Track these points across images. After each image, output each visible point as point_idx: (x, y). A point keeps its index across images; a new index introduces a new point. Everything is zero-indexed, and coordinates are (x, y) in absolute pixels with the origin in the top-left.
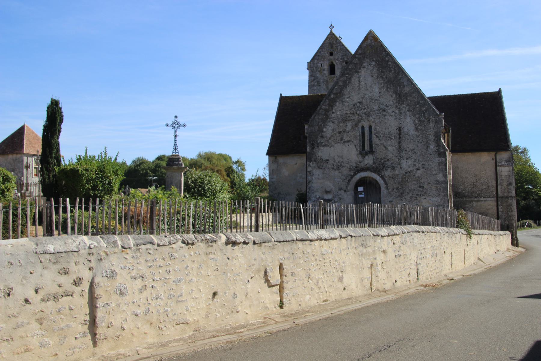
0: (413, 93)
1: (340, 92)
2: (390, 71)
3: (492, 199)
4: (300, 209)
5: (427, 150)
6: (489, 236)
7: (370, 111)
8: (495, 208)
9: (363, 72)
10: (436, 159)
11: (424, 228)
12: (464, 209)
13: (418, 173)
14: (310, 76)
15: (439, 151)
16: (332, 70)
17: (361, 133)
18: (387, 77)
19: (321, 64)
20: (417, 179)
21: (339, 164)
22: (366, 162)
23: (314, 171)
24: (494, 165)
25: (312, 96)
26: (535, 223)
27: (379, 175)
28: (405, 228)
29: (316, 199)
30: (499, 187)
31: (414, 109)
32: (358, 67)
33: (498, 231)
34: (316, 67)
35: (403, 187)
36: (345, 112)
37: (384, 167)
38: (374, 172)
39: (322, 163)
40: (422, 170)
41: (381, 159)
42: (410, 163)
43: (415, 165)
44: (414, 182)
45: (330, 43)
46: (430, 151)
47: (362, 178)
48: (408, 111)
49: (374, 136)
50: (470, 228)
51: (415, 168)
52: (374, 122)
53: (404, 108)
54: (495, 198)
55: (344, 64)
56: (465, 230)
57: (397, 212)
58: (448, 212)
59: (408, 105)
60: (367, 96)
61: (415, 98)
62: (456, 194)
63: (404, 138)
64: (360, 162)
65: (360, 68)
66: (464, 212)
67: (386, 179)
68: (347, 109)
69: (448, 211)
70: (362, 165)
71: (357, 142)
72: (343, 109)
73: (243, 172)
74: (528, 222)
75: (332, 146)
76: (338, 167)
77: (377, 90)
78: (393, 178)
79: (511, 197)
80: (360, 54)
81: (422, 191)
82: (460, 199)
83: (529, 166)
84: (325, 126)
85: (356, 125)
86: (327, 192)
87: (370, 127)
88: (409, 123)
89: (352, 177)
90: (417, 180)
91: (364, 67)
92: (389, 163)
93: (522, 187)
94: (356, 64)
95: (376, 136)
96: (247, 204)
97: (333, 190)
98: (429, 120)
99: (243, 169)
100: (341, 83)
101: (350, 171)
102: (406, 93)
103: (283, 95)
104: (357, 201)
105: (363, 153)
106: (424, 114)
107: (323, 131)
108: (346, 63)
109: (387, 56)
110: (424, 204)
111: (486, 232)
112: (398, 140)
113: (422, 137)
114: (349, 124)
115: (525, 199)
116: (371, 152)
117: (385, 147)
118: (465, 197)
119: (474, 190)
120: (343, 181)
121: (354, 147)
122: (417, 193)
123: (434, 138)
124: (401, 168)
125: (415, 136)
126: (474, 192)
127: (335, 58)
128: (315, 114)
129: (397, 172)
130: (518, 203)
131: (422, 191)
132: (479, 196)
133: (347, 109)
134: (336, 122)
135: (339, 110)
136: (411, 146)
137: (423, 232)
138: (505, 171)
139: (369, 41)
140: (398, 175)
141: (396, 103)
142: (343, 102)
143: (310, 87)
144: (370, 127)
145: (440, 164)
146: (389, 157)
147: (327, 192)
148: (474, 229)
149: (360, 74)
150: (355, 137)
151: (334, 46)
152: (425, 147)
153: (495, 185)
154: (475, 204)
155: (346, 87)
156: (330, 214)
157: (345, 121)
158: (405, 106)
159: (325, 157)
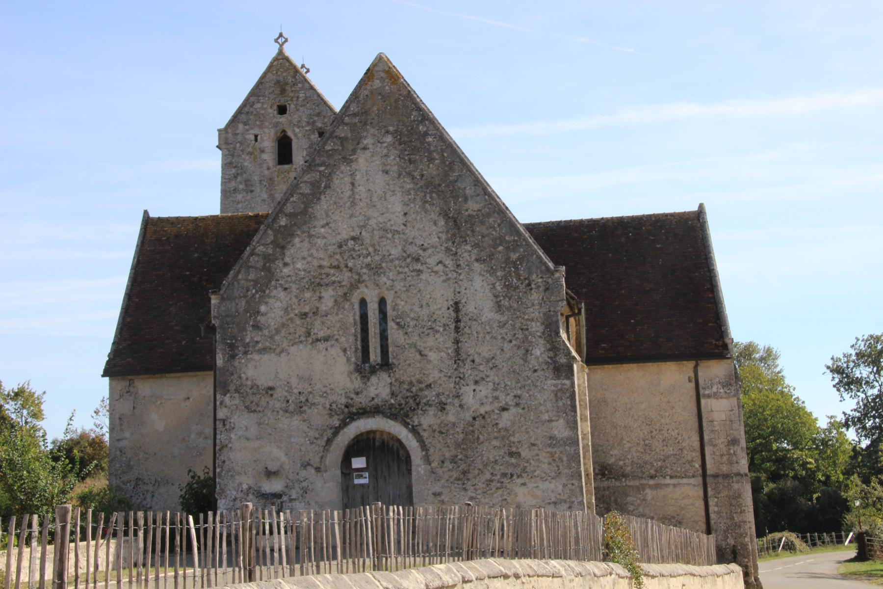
0: (489, 215)
1: (305, 212)
2: (431, 160)
4: (188, 530)
5: (525, 361)
6: (689, 580)
7: (382, 260)
8: (701, 504)
9: (362, 161)
10: (549, 382)
11: (519, 565)
12: (623, 509)
14: (227, 165)
15: (555, 362)
16: (284, 151)
17: (358, 318)
18: (422, 176)
19: (256, 136)
20: (503, 433)
21: (303, 399)
22: (372, 392)
23: (235, 419)
24: (693, 392)
25: (231, 218)
26: (804, 538)
27: (406, 425)
28: (471, 568)
29: (240, 495)
30: (708, 450)
31: (491, 256)
32: (351, 147)
33: (710, 564)
34: (241, 143)
35: (466, 456)
36: (316, 263)
37: (418, 404)
38: (394, 417)
39: (257, 398)
40: (513, 410)
41: (411, 383)
42: (484, 393)
43: (497, 398)
45: (278, 83)
46: (533, 363)
47: (362, 434)
48: (477, 260)
49: (391, 325)
50: (637, 560)
51: (496, 405)
52: (392, 288)
53: (467, 253)
54: (700, 480)
55: (315, 137)
56: (626, 566)
57: (449, 527)
58: (579, 519)
59: (476, 245)
60: (372, 222)
61: (494, 228)
62: (603, 471)
63: (467, 330)
64: (357, 394)
65: (354, 151)
66: (620, 519)
67: (425, 435)
68: (321, 254)
69: (583, 518)
70: (362, 400)
71: (350, 339)
72: (311, 255)
73: (35, 422)
74: (786, 536)
75: (282, 351)
76: (301, 408)
77: (399, 208)
78: (441, 432)
79: (738, 474)
80: (355, 115)
81: (516, 466)
82: (614, 483)
83: (782, 392)
84: (262, 300)
85: (346, 297)
86: (270, 474)
87: (382, 302)
88: (479, 293)
89: (337, 431)
90: (503, 438)
91: (365, 148)
92: (430, 395)
93: (767, 447)
94: (343, 140)
95: (398, 324)
96: (30, 526)
97: (287, 467)
98: (529, 285)
99: (37, 415)
100: (306, 189)
101: (331, 416)
103: (153, 214)
104: (351, 498)
105: (365, 368)
106: (517, 268)
107: (258, 312)
108: (321, 134)
109: (422, 121)
110: (520, 499)
111: (680, 567)
112: (453, 335)
113: (513, 326)
114: (328, 295)
115: (774, 477)
116: (386, 364)
118: (624, 475)
119: (647, 458)
120: (312, 443)
121: (341, 354)
122: (503, 469)
123: (541, 329)
124: (461, 406)
125: (495, 325)
126: (646, 463)
127: (290, 122)
128: (236, 268)
129: (451, 418)
130: (756, 489)
131: (513, 466)
132: (659, 473)
133: (321, 254)
134: (294, 287)
135: (302, 257)
136: (485, 350)
137: (517, 576)
138: (719, 409)
139: (377, 83)
140: (454, 424)
141: (447, 240)
142: (310, 236)
143: (226, 194)
144: (382, 302)
145: (558, 394)
146: (431, 380)
147: (270, 474)
148: (649, 561)
149: (354, 166)
150: (344, 327)
151: (288, 88)
152: (521, 352)
153: (697, 444)
154: (649, 494)
155: (319, 199)
156: (271, 533)
157: (317, 285)
158: (468, 248)
159: (264, 381)
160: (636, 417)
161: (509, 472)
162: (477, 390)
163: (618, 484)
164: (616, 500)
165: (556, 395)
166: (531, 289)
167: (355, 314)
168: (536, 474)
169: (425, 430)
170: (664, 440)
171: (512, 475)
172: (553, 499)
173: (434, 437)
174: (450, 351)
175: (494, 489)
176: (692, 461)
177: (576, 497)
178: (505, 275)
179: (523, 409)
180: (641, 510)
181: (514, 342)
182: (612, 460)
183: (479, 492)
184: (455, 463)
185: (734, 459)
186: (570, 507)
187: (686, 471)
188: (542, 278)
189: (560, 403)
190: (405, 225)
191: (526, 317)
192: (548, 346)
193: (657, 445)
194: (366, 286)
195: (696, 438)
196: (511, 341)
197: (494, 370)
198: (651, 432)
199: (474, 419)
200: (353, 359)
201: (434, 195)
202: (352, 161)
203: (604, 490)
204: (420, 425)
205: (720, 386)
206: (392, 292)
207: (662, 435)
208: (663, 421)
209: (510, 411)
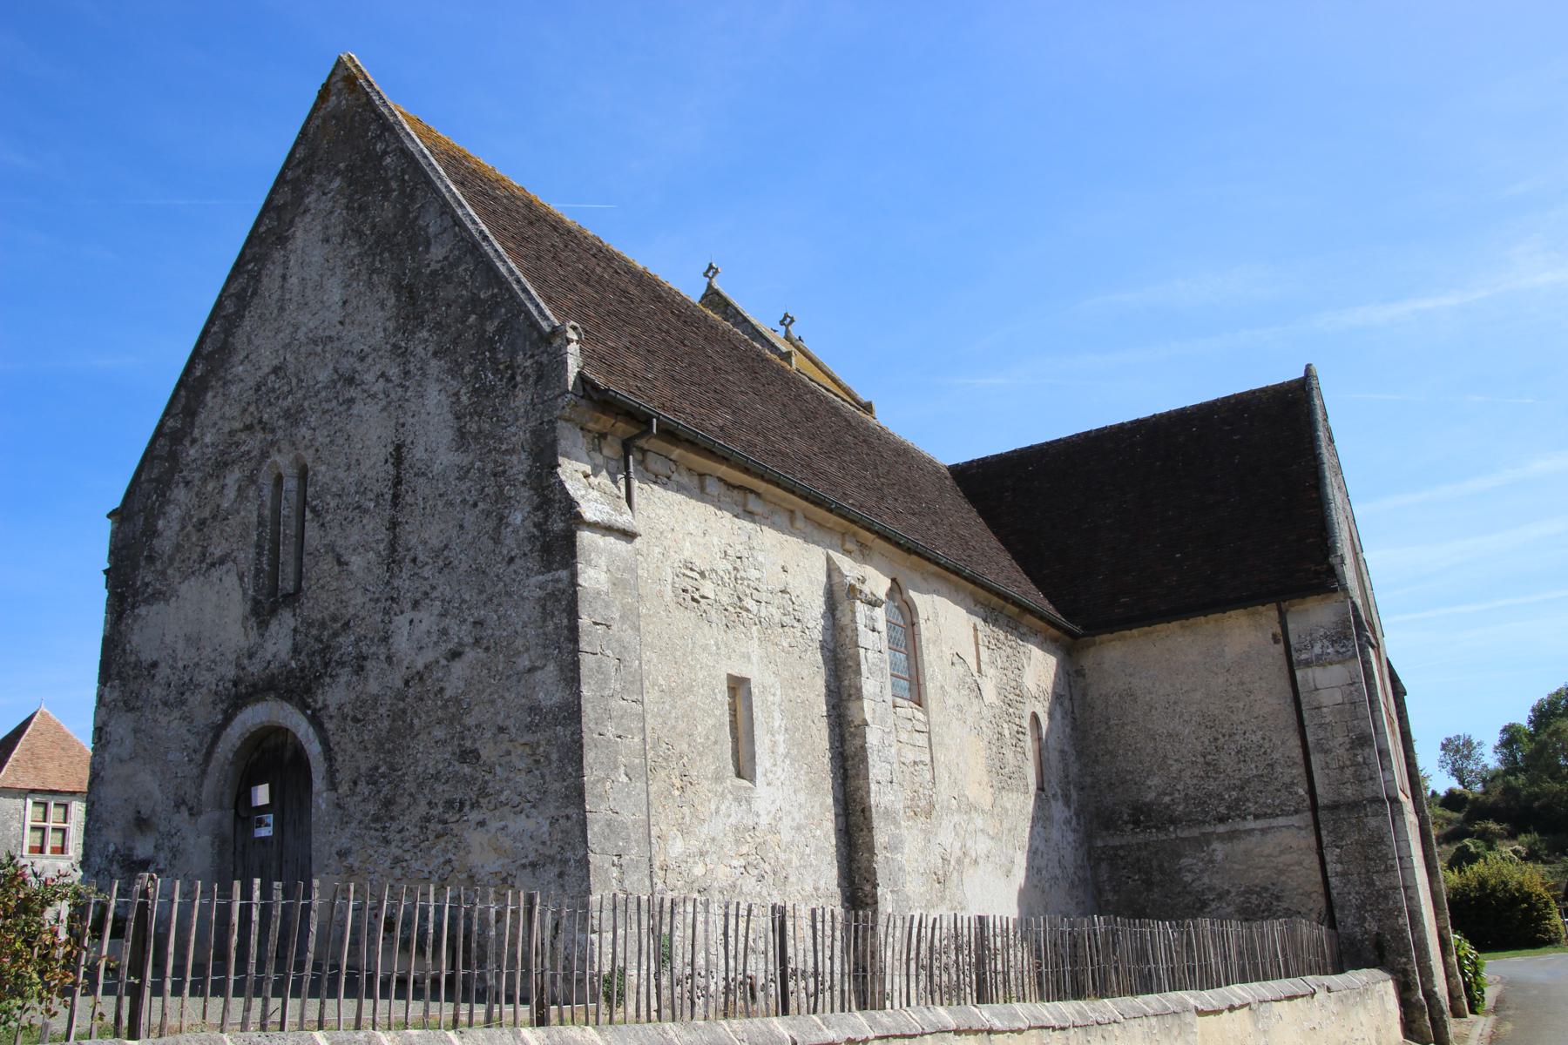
3: (1295, 820)
5: (497, 541)
8: (1312, 861)
13: (457, 677)
15: (545, 533)
18: (374, 227)
24: (1283, 661)
27: (303, 707)
35: (393, 769)
37: (326, 665)
38: (287, 695)
42: (424, 627)
43: (444, 632)
44: (439, 733)
53: (423, 342)
54: (1309, 814)
65: (291, 223)
67: (330, 726)
76: (178, 698)
77: (335, 295)
78: (356, 720)
87: (303, 474)
89: (218, 730)
92: (346, 642)
98: (513, 377)
102: (434, 273)
112: (388, 513)
117: (340, 562)
118: (1174, 821)
119: (1212, 786)
122: (443, 791)
126: (1210, 795)
129: (373, 687)
132: (1236, 809)
136: (434, 534)
140: (375, 698)
141: (397, 329)
152: (490, 525)
153: (1297, 753)
154: (1219, 849)
158: (425, 334)
160: (1186, 717)
161: (458, 796)
162: (416, 621)
163: (1162, 836)
164: (1161, 866)
165: (544, 607)
166: (515, 386)
167: (261, 505)
168: (503, 798)
169: (331, 717)
170: (1238, 752)
171: (462, 804)
172: (532, 857)
173: (344, 731)
174: (382, 547)
175: (431, 838)
176: (1293, 783)
177: (574, 849)
178: (476, 370)
179: (487, 649)
180: (1206, 880)
181: (481, 505)
182: (1151, 796)
183: (408, 845)
184: (375, 783)
185: (1366, 771)
186: (561, 875)
187: (1282, 803)
188: (532, 356)
189: (550, 627)
190: (341, 323)
191: (504, 447)
192: (536, 500)
193: (1227, 761)
194: (279, 451)
195: (1294, 742)
196: (475, 505)
197: (446, 570)
198: (1216, 739)
199: (407, 683)
200: (251, 592)
201: (386, 255)
202: (287, 239)
203: (1139, 849)
204: (326, 707)
205: (1327, 643)
206: (311, 451)
207: (1235, 742)
208: (1234, 718)
209: (465, 658)
